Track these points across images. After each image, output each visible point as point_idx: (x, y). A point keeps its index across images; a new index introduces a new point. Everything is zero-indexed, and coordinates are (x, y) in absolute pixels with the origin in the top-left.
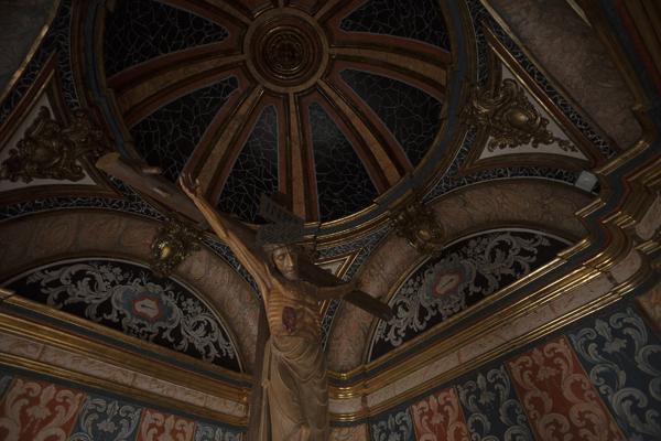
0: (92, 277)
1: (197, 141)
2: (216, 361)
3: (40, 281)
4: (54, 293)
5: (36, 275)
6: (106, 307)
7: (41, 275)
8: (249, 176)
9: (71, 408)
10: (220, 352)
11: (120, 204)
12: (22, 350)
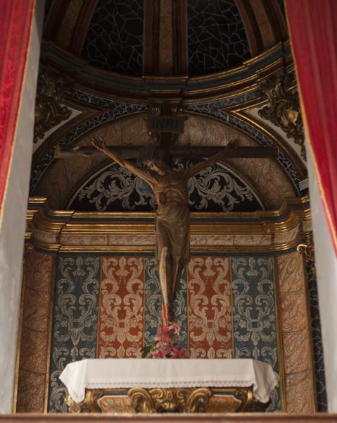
0: (116, 178)
1: (141, 14)
2: (237, 208)
3: (86, 196)
4: (97, 200)
5: (81, 192)
6: (134, 196)
7: (84, 191)
8: (207, 16)
9: (139, 268)
10: (239, 198)
11: (106, 115)
12: (97, 242)
